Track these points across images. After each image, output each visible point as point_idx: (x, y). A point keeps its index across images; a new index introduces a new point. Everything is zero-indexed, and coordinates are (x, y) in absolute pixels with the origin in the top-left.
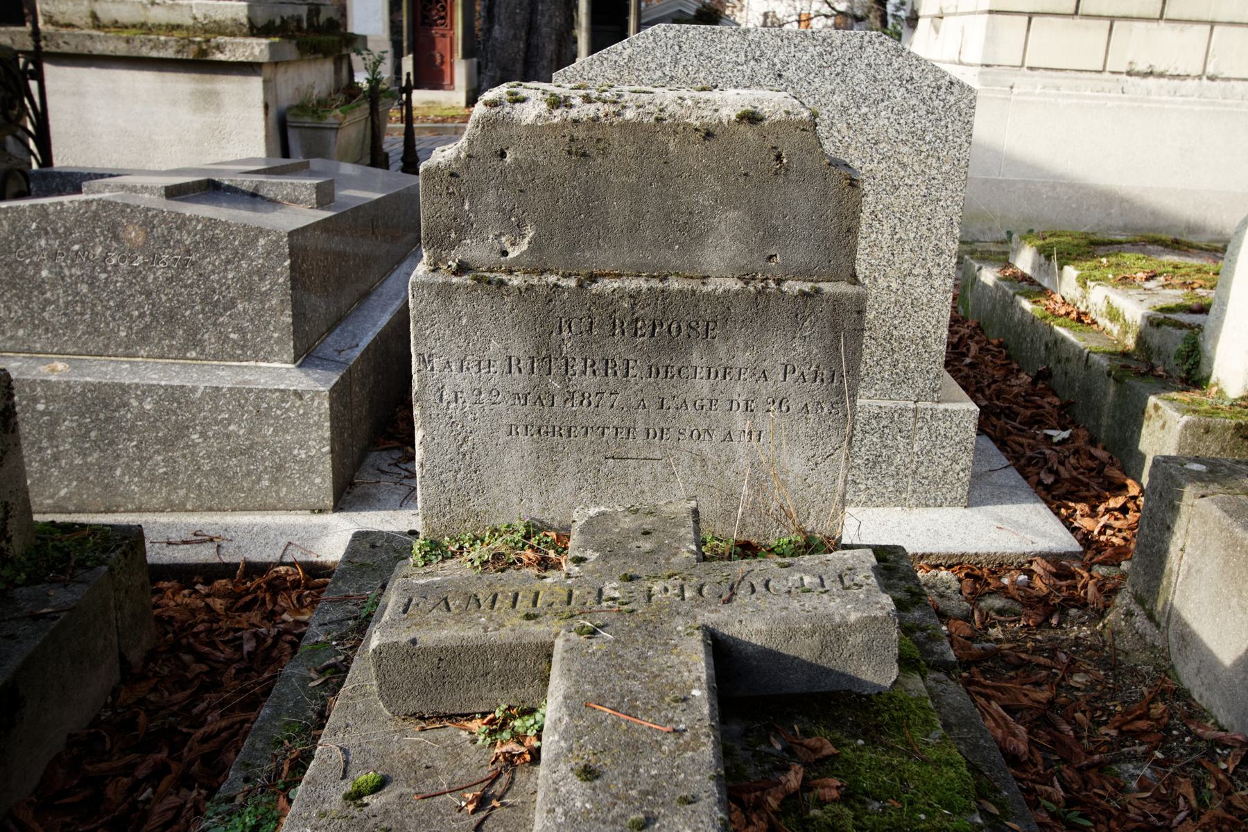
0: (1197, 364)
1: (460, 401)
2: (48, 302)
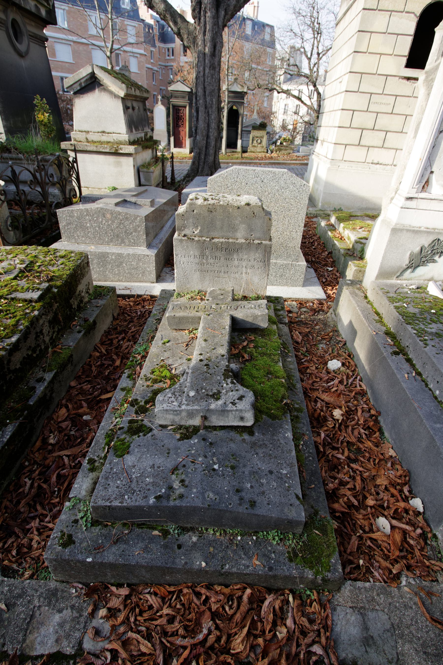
0: (363, 254)
2: (89, 232)
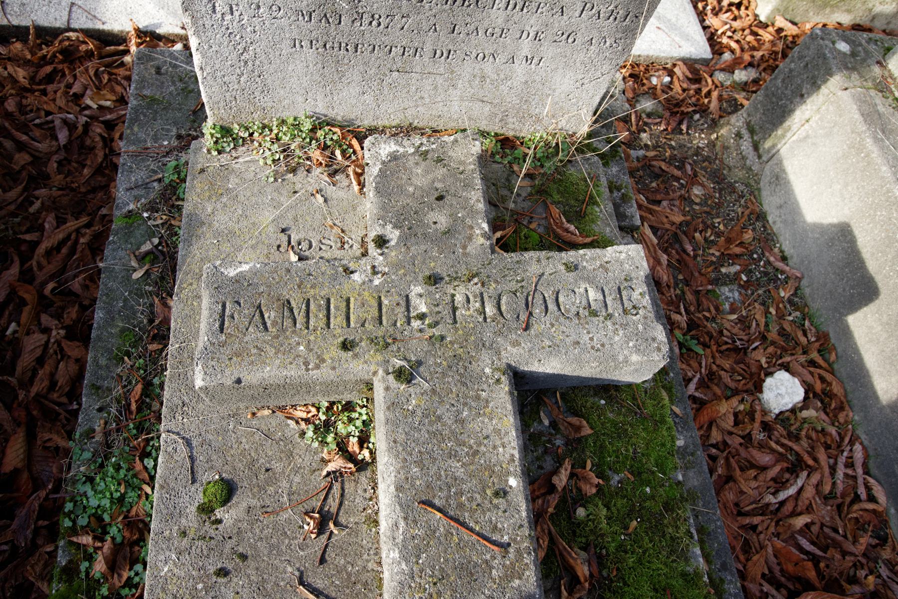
1: (236, 14)
